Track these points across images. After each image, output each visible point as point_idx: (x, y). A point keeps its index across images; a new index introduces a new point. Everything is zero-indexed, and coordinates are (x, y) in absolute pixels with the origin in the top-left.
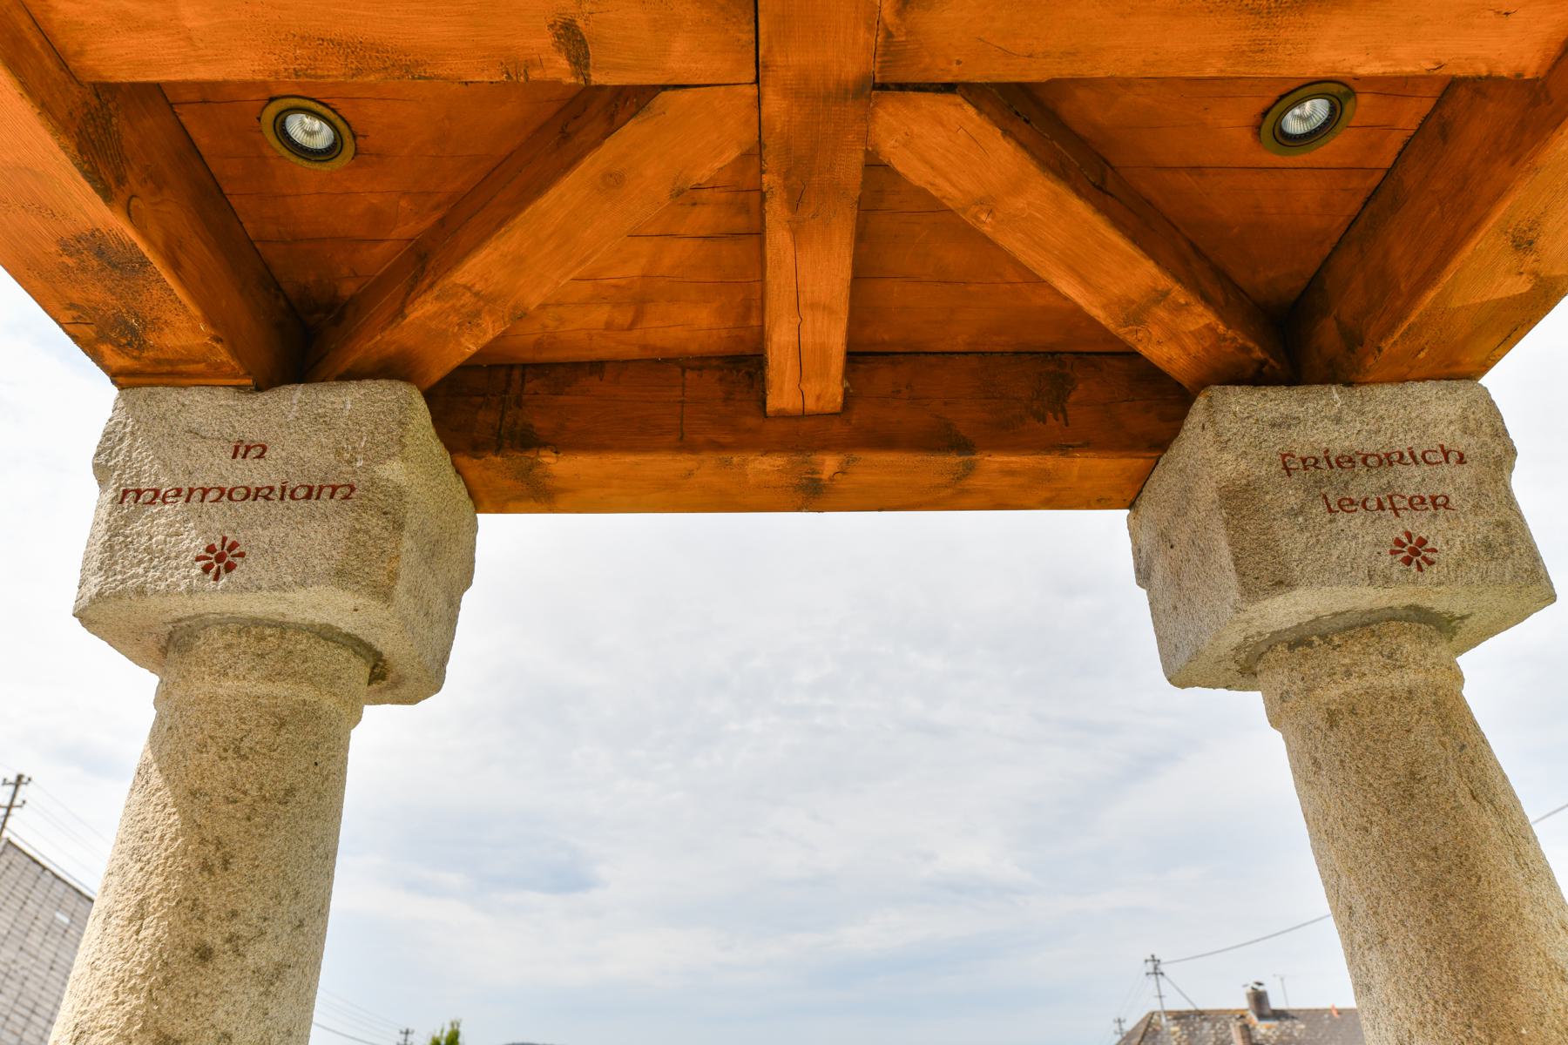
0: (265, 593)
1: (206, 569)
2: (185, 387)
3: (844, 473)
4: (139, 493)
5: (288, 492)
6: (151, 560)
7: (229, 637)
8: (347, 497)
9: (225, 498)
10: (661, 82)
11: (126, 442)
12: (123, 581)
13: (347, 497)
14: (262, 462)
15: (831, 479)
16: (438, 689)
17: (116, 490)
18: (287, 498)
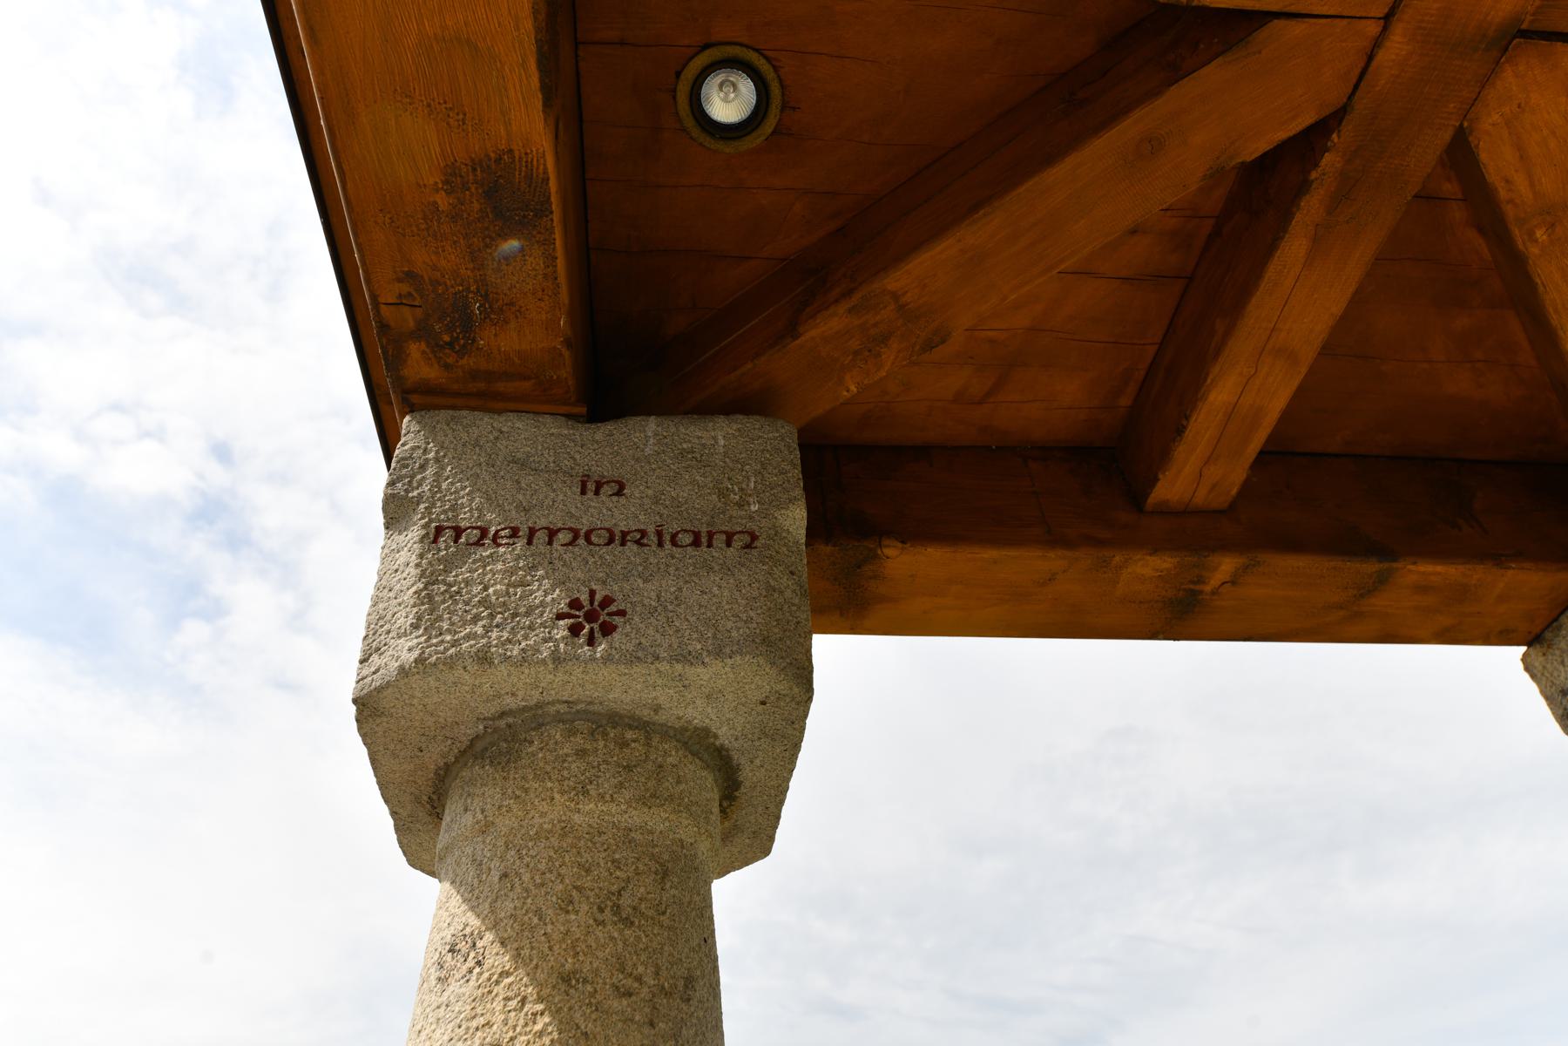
0: (664, 667)
1: (575, 630)
2: (500, 412)
3: (1233, 583)
4: (458, 532)
5: (667, 538)
6: (492, 616)
7: (579, 739)
8: (748, 546)
9: (581, 541)
10: (1274, 8)
11: (430, 471)
12: (455, 643)
13: (748, 546)
14: (623, 500)
15: (1214, 592)
16: (765, 851)
17: (425, 526)
18: (668, 545)
